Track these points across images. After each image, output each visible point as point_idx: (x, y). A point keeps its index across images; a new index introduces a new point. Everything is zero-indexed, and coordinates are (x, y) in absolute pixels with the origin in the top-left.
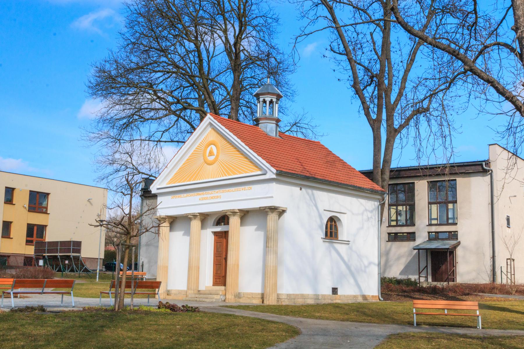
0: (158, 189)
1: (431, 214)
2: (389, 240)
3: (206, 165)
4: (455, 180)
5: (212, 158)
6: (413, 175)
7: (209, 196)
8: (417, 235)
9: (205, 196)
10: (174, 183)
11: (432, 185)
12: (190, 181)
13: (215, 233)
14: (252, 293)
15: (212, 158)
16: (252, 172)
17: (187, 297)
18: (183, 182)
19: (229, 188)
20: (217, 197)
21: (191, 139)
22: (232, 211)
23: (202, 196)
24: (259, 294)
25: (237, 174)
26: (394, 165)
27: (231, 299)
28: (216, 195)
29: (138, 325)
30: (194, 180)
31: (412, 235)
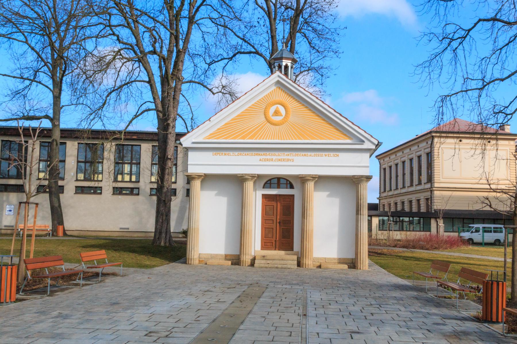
0: (193, 143)
1: (455, 188)
2: (113, 193)
3: (268, 124)
4: (140, 145)
5: (278, 119)
6: (147, 139)
7: (274, 158)
8: (65, 188)
9: (268, 157)
10: (217, 138)
11: (120, 149)
12: (252, 139)
13: (265, 196)
14: (325, 258)
15: (278, 119)
16: (338, 139)
17: (2, 257)
18: (232, 139)
19: (300, 152)
20: (288, 160)
21: (250, 95)
22: (311, 176)
23: (264, 157)
24: (334, 259)
25: (302, 140)
26: (62, 126)
27: (310, 265)
28: (268, 157)
29: (140, 303)
30: (251, 138)
31: (62, 188)
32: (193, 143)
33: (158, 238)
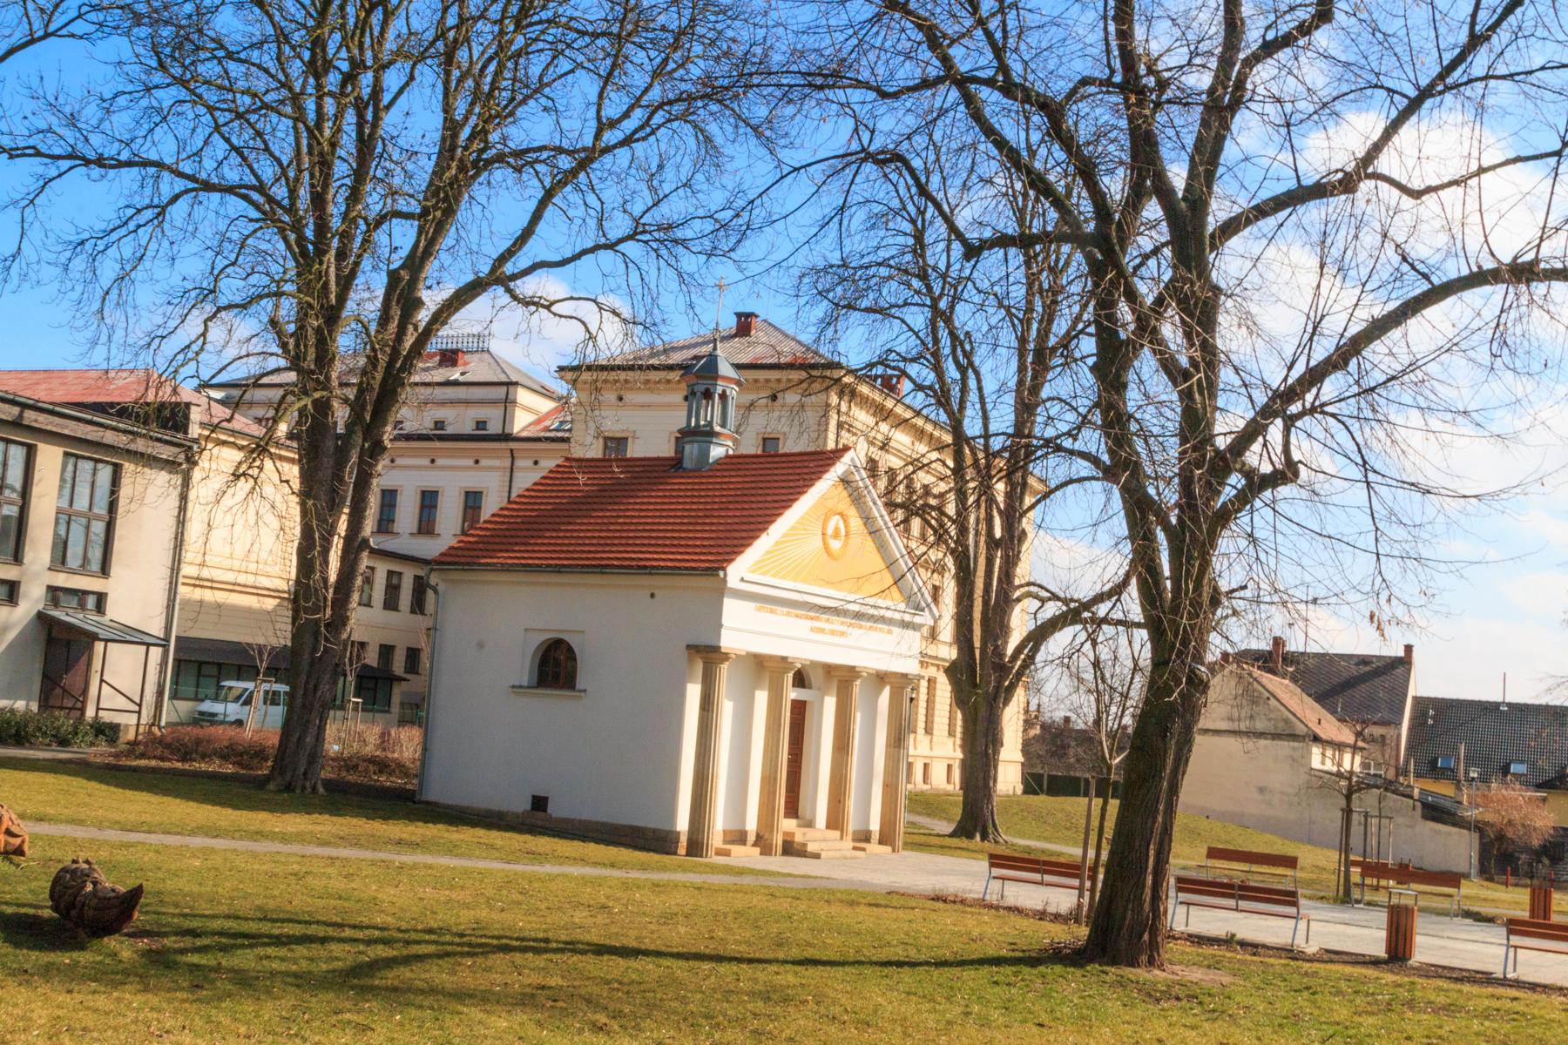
32: (742, 580)
33: (305, 774)
